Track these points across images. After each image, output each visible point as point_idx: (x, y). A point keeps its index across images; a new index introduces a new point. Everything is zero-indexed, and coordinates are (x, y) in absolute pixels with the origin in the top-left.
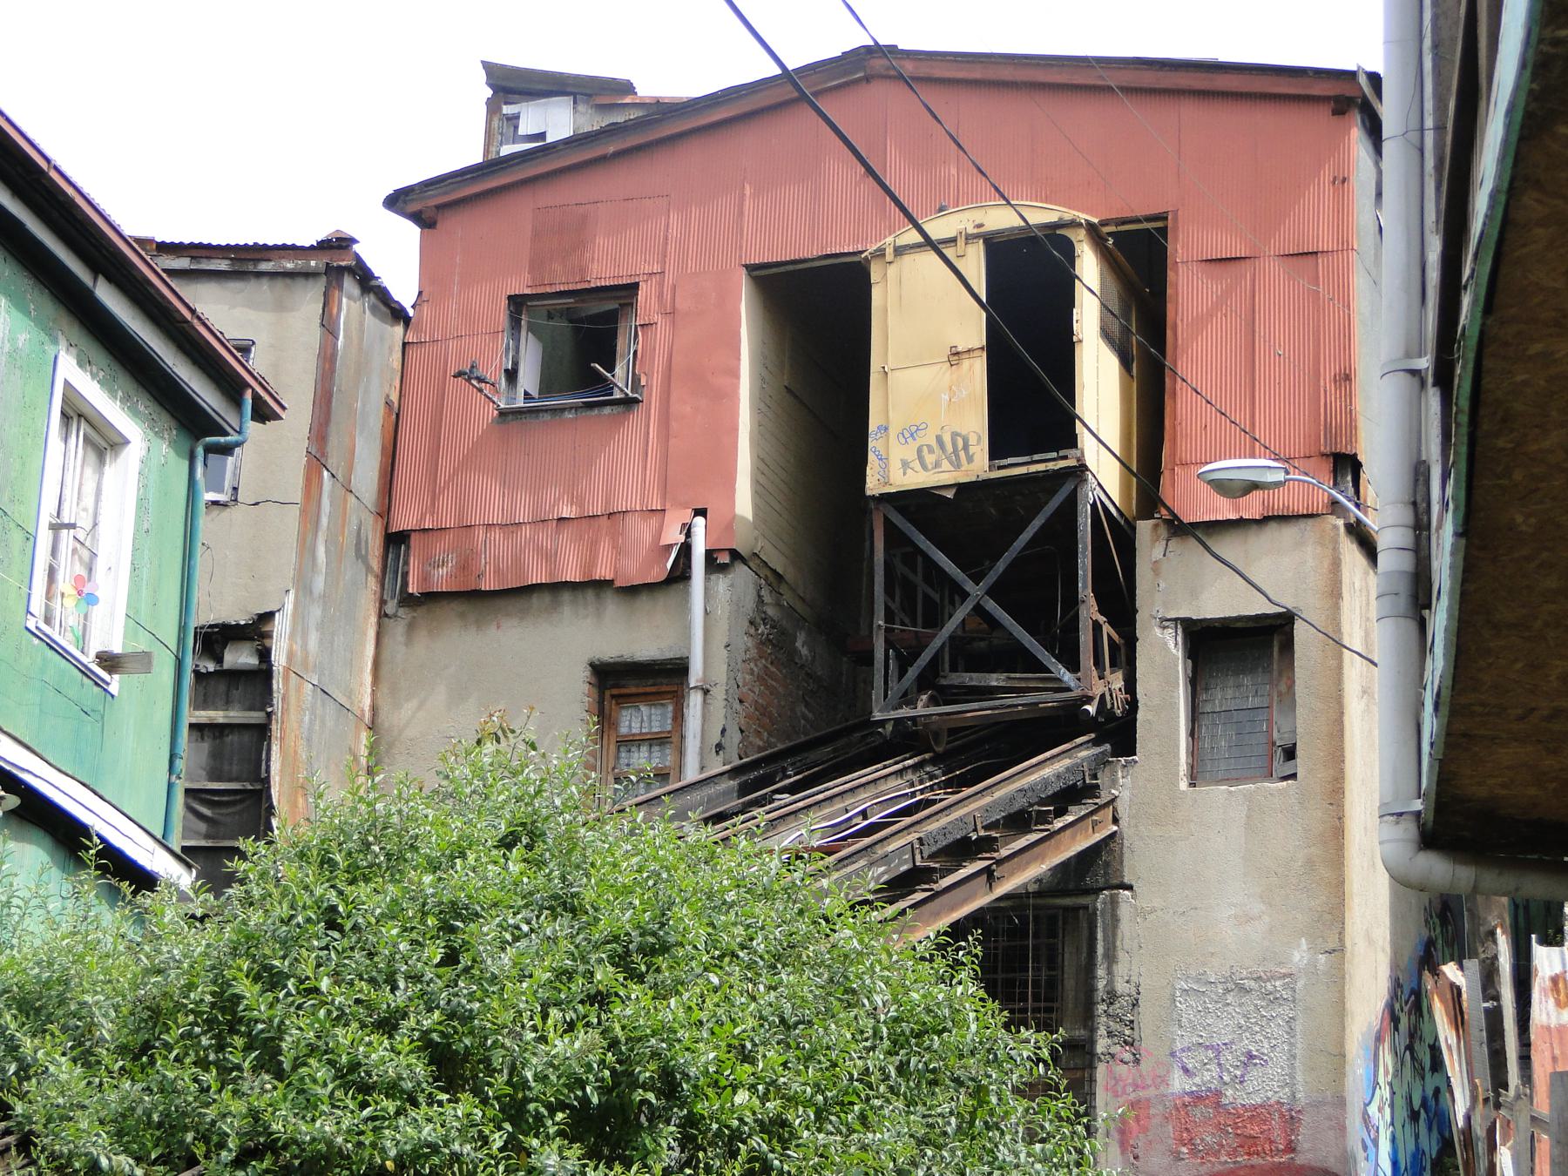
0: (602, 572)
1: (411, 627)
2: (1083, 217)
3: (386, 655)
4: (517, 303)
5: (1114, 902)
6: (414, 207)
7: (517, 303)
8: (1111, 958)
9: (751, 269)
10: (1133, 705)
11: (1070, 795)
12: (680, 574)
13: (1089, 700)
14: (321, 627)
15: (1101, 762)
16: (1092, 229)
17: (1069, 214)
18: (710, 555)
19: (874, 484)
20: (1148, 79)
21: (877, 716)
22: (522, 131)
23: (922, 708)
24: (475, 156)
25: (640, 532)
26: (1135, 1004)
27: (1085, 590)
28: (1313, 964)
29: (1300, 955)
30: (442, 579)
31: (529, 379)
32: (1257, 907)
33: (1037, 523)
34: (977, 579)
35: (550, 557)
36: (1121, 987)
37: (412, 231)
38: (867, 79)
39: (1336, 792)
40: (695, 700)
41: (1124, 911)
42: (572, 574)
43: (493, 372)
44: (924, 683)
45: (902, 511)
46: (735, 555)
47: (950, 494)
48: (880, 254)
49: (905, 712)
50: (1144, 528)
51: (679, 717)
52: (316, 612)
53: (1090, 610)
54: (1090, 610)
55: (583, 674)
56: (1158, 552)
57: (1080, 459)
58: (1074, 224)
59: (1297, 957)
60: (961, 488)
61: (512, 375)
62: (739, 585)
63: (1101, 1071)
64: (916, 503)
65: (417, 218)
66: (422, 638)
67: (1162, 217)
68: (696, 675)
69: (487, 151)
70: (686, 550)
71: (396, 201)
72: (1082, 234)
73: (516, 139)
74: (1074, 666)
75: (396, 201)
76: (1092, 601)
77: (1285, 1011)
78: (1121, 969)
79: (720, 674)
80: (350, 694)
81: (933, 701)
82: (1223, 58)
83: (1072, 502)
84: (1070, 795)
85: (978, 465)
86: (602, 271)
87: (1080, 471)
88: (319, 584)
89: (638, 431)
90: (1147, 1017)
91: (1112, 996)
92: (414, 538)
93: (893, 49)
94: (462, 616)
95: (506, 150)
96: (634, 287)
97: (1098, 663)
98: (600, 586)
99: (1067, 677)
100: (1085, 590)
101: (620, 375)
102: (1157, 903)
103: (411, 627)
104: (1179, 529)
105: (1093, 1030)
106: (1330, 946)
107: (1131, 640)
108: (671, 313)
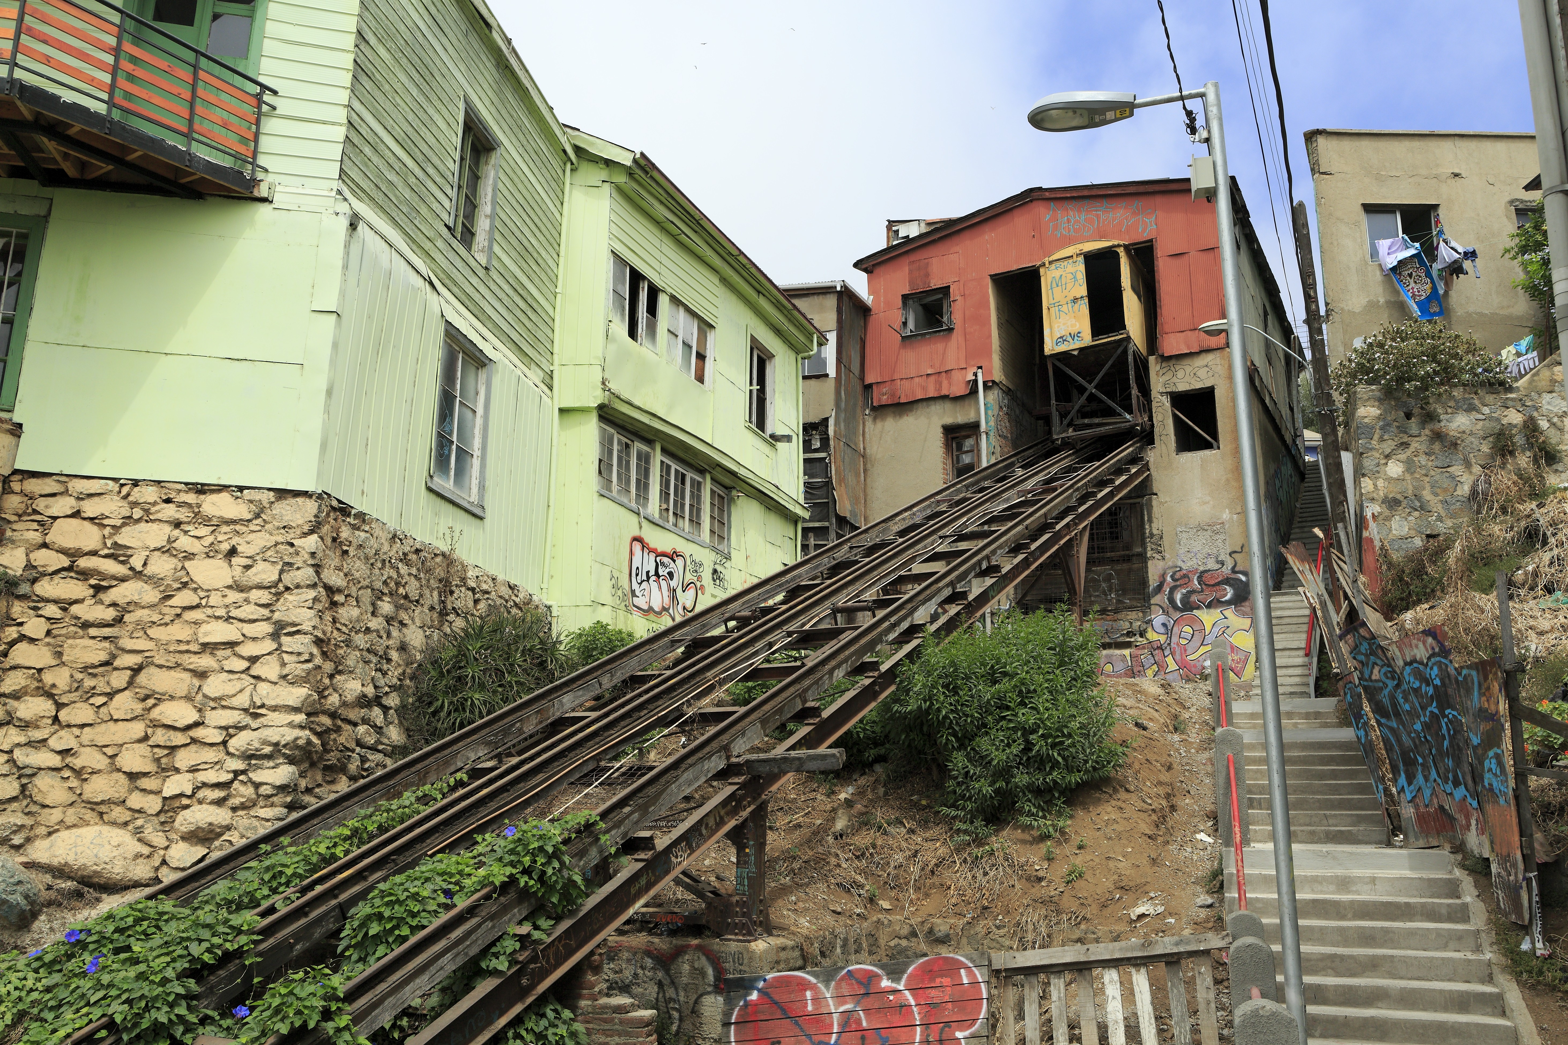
0: (945, 392)
1: (875, 419)
2: (1121, 243)
3: (867, 430)
4: (905, 298)
5: (1150, 500)
6: (864, 266)
7: (905, 298)
8: (1150, 521)
9: (992, 276)
10: (1152, 426)
11: (1134, 460)
12: (974, 391)
13: (1137, 425)
14: (845, 421)
15: (1141, 449)
16: (1126, 248)
17: (1116, 243)
18: (985, 383)
19: (1050, 347)
20: (1141, 189)
21: (1055, 437)
22: (900, 235)
23: (1071, 432)
24: (884, 246)
25: (957, 376)
26: (1161, 538)
27: (1133, 382)
28: (1231, 518)
29: (1226, 515)
30: (885, 400)
31: (911, 325)
32: (1208, 498)
33: (1110, 363)
34: (1090, 382)
35: (924, 389)
36: (1155, 532)
37: (864, 275)
38: (1031, 201)
39: (1237, 451)
40: (984, 436)
41: (1154, 503)
42: (931, 394)
43: (897, 325)
44: (1070, 425)
45: (1059, 360)
46: (994, 382)
47: (1076, 353)
48: (1044, 265)
49: (1064, 435)
50: (1152, 359)
51: (978, 444)
52: (843, 415)
53: (1135, 391)
54: (1135, 391)
55: (940, 430)
56: (1158, 367)
57: (1128, 333)
58: (1119, 246)
59: (1225, 516)
60: (1081, 350)
61: (905, 324)
62: (994, 395)
63: (1150, 563)
64: (1064, 357)
65: (865, 270)
66: (879, 424)
67: (1151, 241)
68: (983, 426)
69: (888, 241)
70: (975, 382)
71: (857, 265)
72: (1122, 249)
73: (897, 238)
74: (1130, 412)
75: (857, 265)
76: (1135, 387)
77: (1222, 537)
78: (1154, 525)
79: (992, 423)
80: (856, 444)
81: (1075, 430)
82: (1172, 177)
83: (1125, 352)
84: (1134, 460)
85: (1086, 339)
86: (936, 283)
87: (1128, 338)
88: (843, 405)
89: (957, 337)
90: (1166, 542)
91: (1152, 535)
92: (874, 387)
93: (1040, 189)
94: (894, 413)
95: (895, 243)
96: (949, 287)
97: (1140, 411)
98: (945, 398)
99: (1128, 416)
100: (1133, 382)
101: (945, 319)
102: (1168, 499)
103: (875, 419)
104: (1165, 359)
105: (1145, 549)
106: (1239, 510)
107: (1150, 402)
108: (963, 295)
